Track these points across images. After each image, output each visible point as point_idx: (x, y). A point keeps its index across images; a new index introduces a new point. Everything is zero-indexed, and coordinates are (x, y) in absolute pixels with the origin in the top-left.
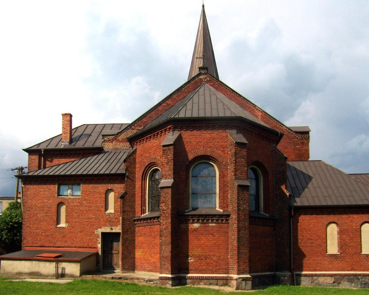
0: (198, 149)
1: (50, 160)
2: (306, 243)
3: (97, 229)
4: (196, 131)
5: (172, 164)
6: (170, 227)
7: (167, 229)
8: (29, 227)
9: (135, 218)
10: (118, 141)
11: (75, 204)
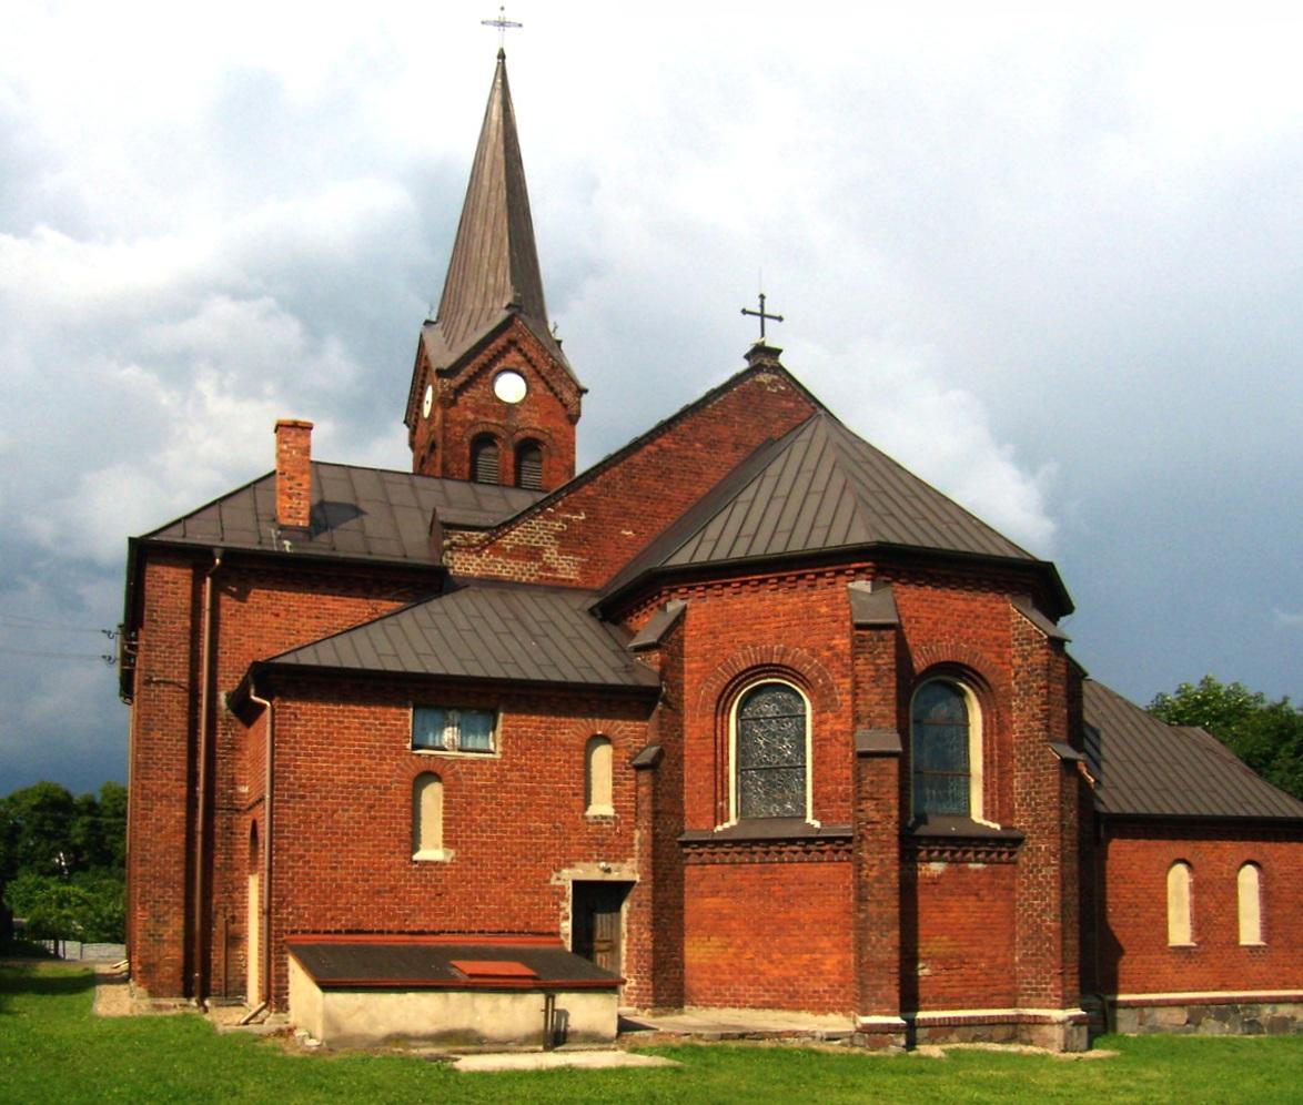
0: (938, 641)
1: (234, 589)
2: (1124, 915)
3: (559, 871)
4: (930, 588)
5: (893, 684)
6: (894, 875)
7: (885, 880)
8: (302, 857)
9: (683, 839)
10: (499, 551)
11: (477, 780)
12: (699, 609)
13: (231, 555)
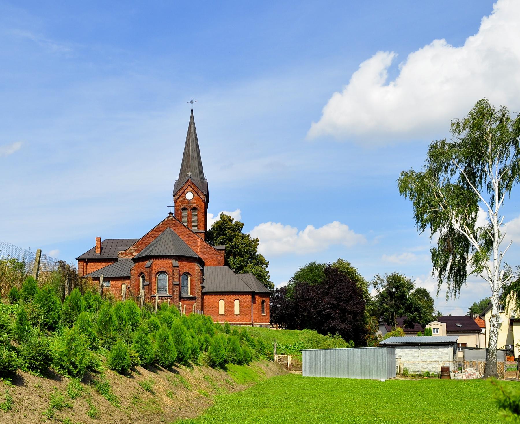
10: (126, 254)
12: (155, 262)
13: (88, 259)
